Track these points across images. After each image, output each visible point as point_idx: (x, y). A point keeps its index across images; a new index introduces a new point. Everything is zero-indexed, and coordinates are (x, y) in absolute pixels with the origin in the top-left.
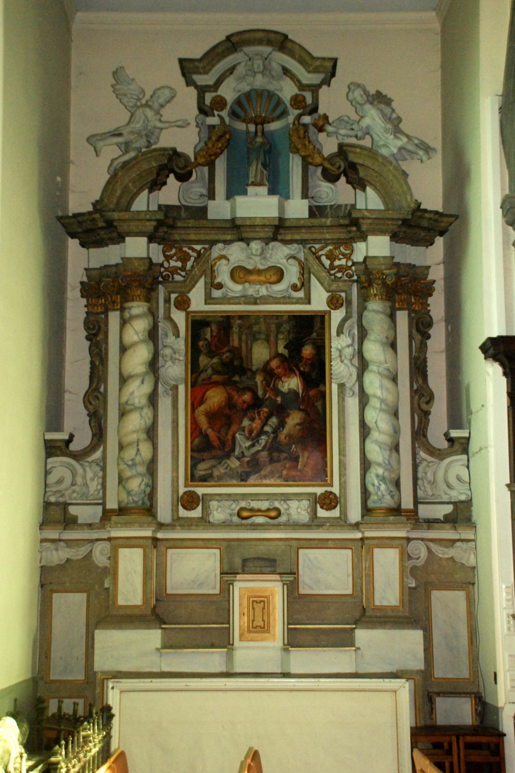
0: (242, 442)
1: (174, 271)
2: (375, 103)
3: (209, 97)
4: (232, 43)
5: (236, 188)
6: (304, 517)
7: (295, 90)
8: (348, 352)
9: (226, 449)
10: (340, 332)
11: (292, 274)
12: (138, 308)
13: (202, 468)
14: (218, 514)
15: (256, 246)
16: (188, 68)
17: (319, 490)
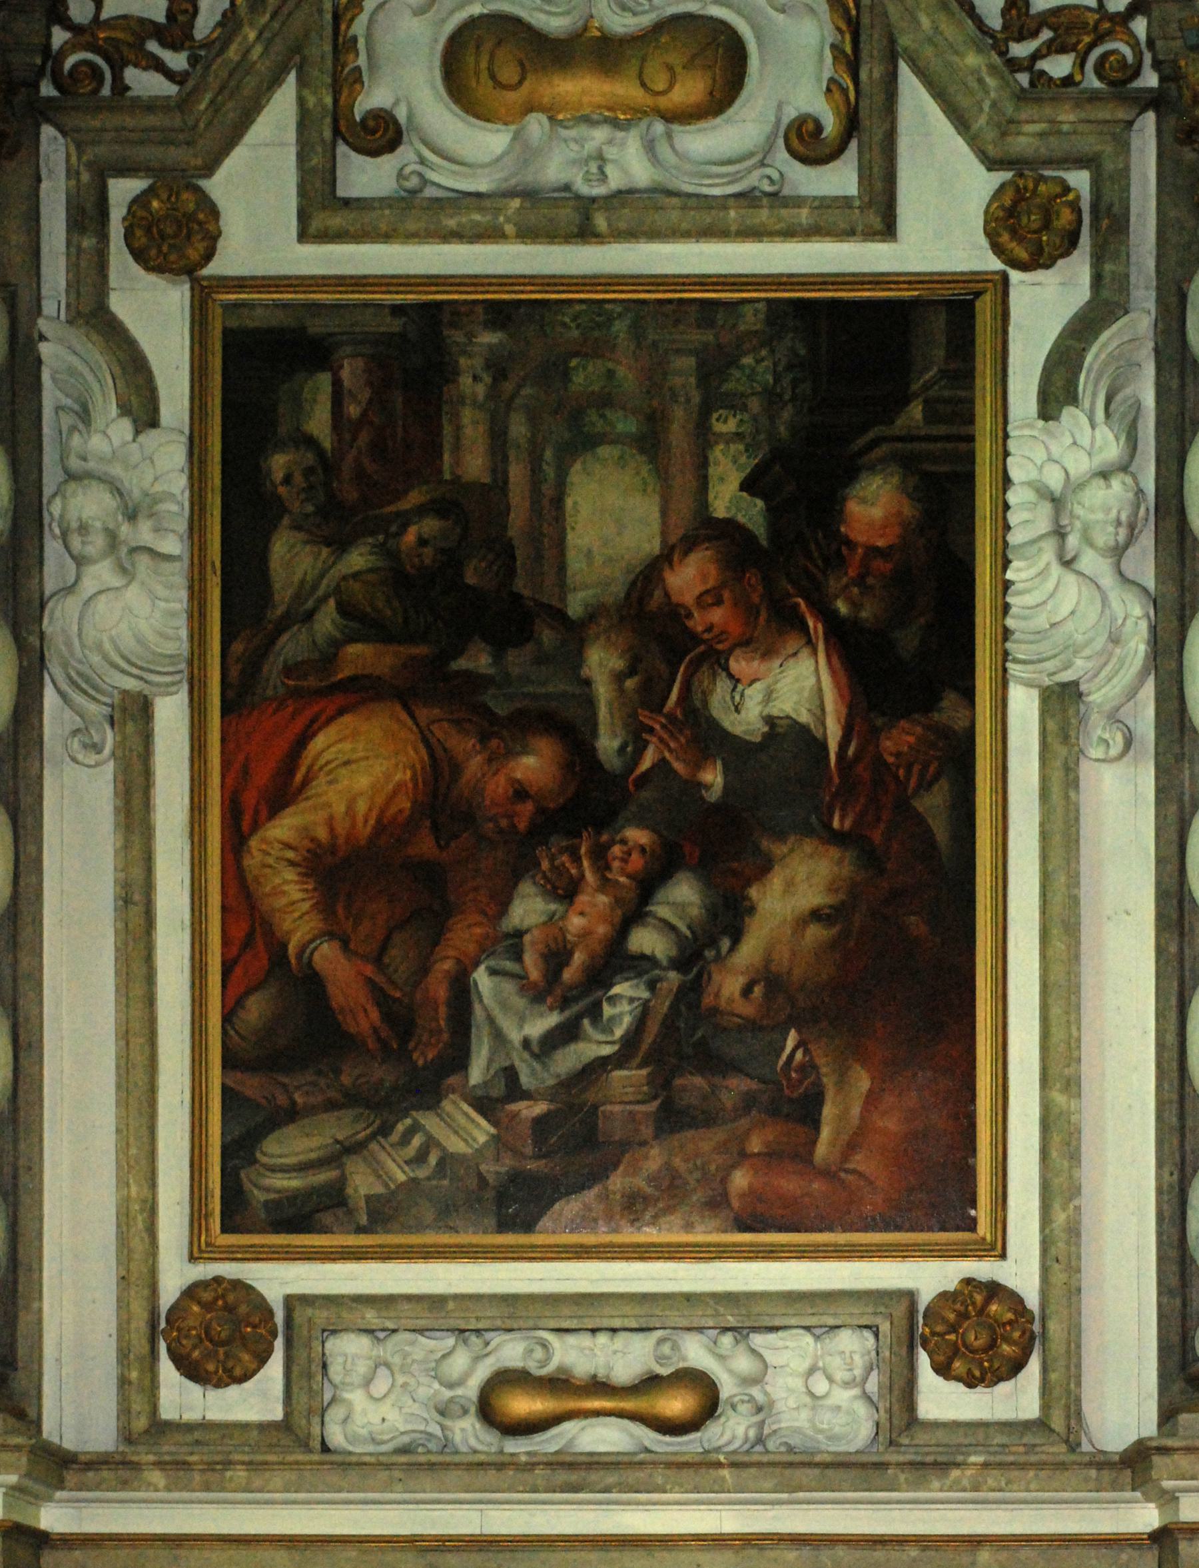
0: (509, 1017)
9: (416, 1055)
10: (1057, 394)
14: (375, 1402)
17: (930, 1277)
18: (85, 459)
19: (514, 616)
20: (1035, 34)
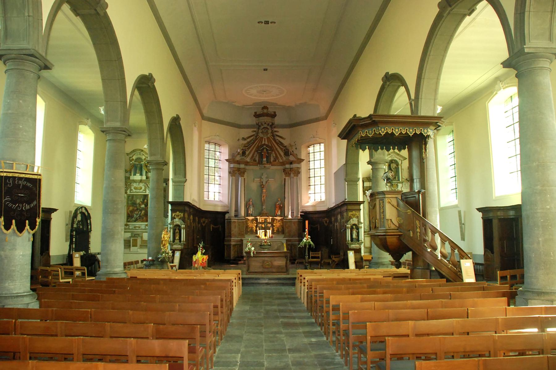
0: (135, 216)
4: (134, 151)
5: (135, 175)
9: (132, 217)
11: (143, 188)
13: (129, 220)
14: (130, 228)
20: (202, 358)
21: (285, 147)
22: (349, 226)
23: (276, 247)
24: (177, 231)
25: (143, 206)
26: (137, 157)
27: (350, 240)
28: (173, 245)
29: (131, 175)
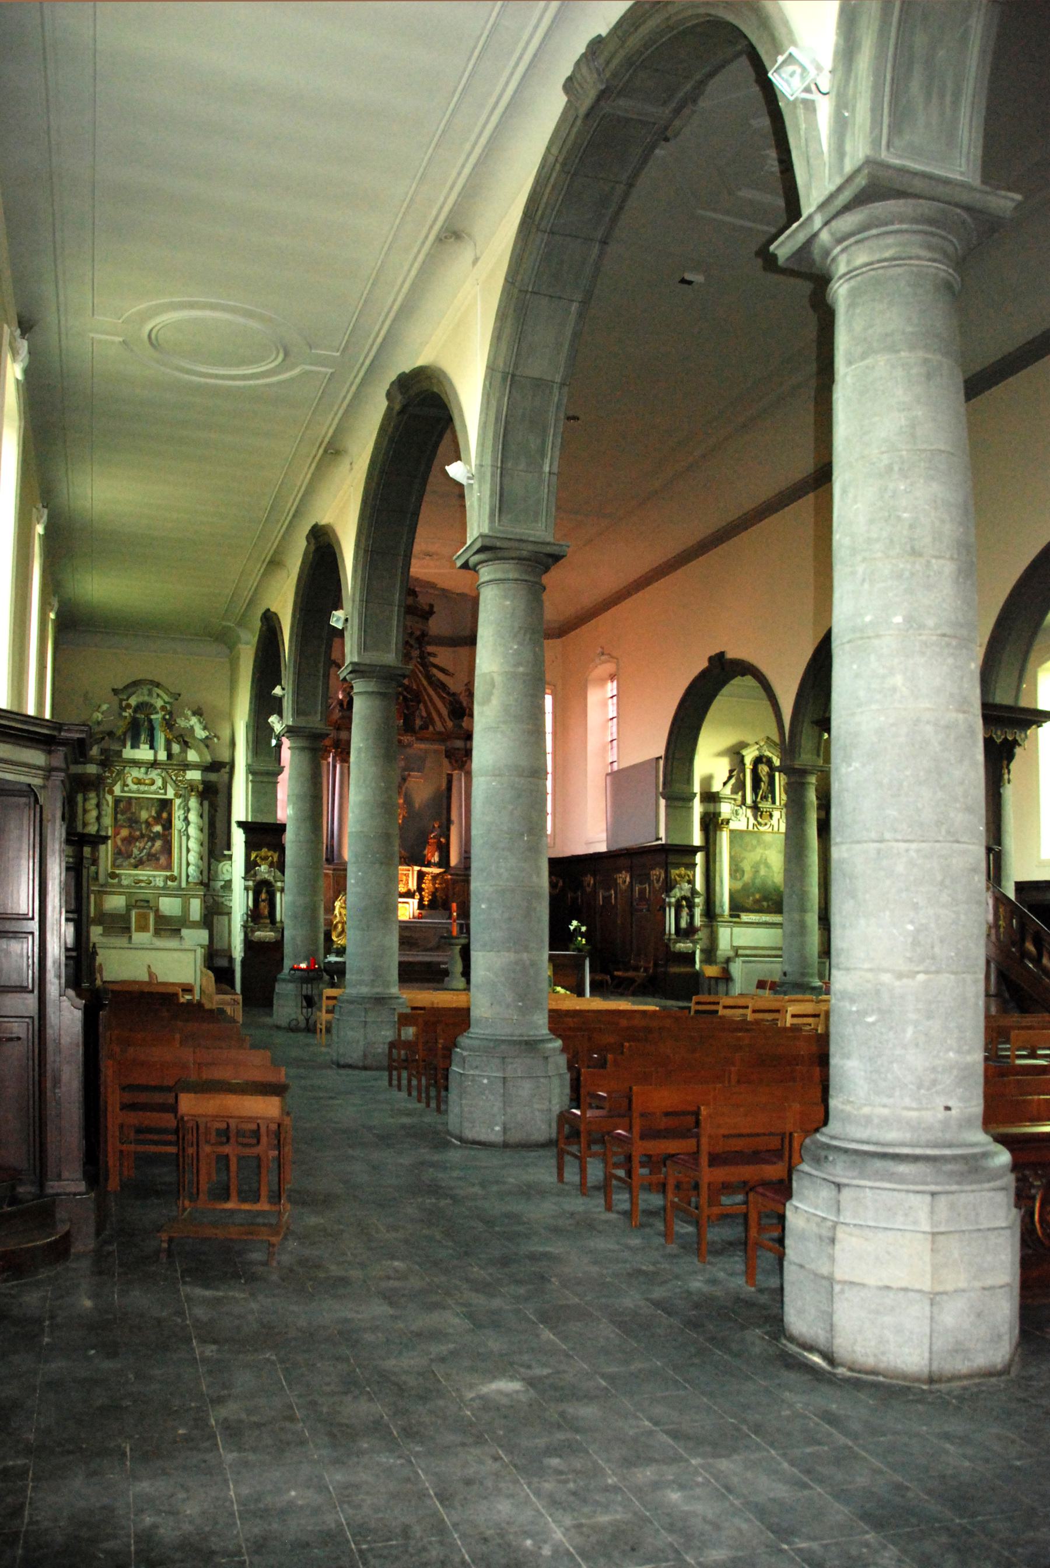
0: (136, 851)
1: (108, 777)
2: (512, 975)
3: (124, 703)
4: (136, 684)
5: (135, 746)
6: (161, 884)
7: (162, 703)
8: (182, 817)
10: (179, 808)
11: (159, 782)
12: (92, 795)
13: (119, 862)
14: (125, 882)
15: (143, 770)
16: (115, 691)
17: (168, 874)
18: (999, 1336)
19: (137, 822)
21: (454, 694)
22: (673, 900)
23: (433, 943)
24: (263, 896)
25: (158, 828)
26: (141, 699)
27: (673, 931)
28: (253, 931)
29: (124, 746)
